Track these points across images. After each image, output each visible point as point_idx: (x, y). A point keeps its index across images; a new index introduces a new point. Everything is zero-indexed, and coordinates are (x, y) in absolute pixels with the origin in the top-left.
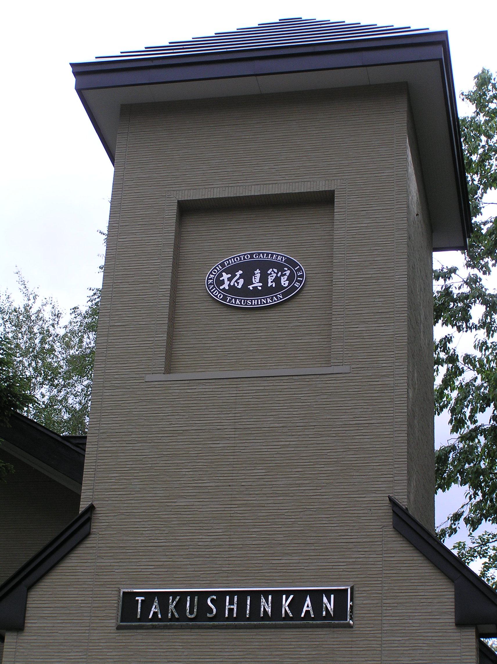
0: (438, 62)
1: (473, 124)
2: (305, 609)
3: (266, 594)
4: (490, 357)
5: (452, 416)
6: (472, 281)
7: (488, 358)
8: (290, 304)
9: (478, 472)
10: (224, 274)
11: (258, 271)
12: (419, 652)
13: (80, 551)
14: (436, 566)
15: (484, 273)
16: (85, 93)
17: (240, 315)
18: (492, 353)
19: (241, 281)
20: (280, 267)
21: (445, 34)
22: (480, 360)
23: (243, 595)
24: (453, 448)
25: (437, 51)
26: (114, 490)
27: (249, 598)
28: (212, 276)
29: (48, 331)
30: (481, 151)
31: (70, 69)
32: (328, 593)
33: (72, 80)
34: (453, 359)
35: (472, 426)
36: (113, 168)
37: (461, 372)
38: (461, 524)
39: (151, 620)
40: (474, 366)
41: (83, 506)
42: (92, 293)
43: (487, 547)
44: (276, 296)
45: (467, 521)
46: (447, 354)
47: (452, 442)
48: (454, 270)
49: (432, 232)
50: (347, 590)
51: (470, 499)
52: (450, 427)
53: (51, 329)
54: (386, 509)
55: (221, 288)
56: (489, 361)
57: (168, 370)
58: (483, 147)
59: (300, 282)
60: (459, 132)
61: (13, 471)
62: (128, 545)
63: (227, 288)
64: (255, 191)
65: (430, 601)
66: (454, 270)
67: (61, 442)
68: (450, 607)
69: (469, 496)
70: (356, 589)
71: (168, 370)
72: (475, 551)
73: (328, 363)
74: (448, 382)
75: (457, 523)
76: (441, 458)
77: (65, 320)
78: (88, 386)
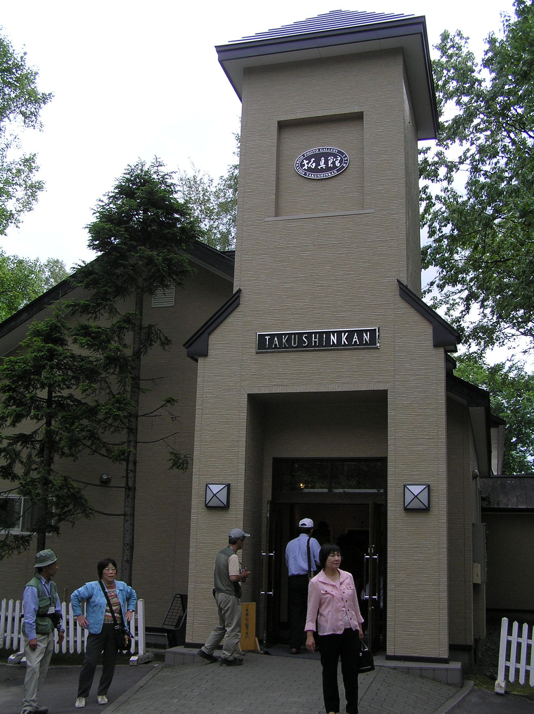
0: (420, 35)
1: (439, 63)
2: (354, 340)
3: (333, 333)
4: (450, 196)
5: (429, 229)
6: (439, 154)
7: (448, 196)
8: (341, 176)
9: (444, 259)
10: (304, 160)
11: (323, 158)
12: (414, 361)
13: (235, 314)
14: (423, 315)
15: (446, 149)
16: (225, 63)
17: (314, 183)
18: (451, 194)
19: (314, 164)
20: (335, 156)
21: (424, 17)
22: (445, 198)
23: (321, 334)
24: (430, 247)
25: (420, 28)
26: (251, 280)
27: (324, 335)
28: (298, 162)
29: (207, 189)
30: (443, 79)
31: (215, 49)
32: (366, 331)
33: (216, 56)
34: (429, 198)
35: (440, 235)
36: (241, 104)
37: (434, 205)
38: (435, 288)
39: (274, 348)
40: (441, 201)
41: (235, 290)
42: (230, 167)
43: (448, 299)
44: (333, 172)
45: (438, 286)
46: (426, 195)
47: (429, 244)
48: (429, 149)
49: (417, 130)
50: (376, 329)
51: (440, 274)
52: (428, 235)
53: (208, 188)
54: (396, 287)
55: (303, 168)
56: (449, 198)
57: (277, 215)
58: (445, 76)
59: (346, 163)
60: (431, 68)
61: (197, 272)
62: (259, 309)
63: (306, 168)
64: (320, 114)
65: (420, 334)
66: (429, 149)
67: (220, 255)
68: (430, 337)
69: (439, 272)
70: (380, 328)
71: (277, 215)
72: (442, 301)
73: (363, 208)
74: (426, 211)
75: (432, 287)
76: (424, 252)
77: (215, 183)
78: (230, 220)
